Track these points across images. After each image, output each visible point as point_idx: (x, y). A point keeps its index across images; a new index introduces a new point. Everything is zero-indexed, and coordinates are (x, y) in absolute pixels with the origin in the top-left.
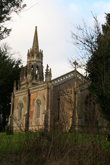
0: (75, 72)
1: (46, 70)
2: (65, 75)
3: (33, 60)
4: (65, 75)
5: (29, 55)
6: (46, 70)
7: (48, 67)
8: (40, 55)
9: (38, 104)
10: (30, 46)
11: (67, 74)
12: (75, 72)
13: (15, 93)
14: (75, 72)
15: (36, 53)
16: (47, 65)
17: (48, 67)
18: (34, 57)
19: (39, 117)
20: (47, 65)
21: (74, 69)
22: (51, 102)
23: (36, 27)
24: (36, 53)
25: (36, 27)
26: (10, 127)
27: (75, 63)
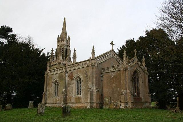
0: (113, 51)
1: (73, 53)
2: (99, 57)
3: (63, 44)
4: (105, 54)
5: (58, 40)
6: (73, 53)
7: (76, 50)
8: (68, 40)
9: (78, 81)
10: (59, 33)
11: (104, 54)
12: (112, 51)
13: (48, 72)
14: (112, 51)
15: (64, 40)
16: (75, 49)
17: (75, 50)
18: (63, 42)
19: (56, 95)
20: (75, 49)
21: (111, 49)
22: (96, 79)
23: (65, 18)
24: (64, 40)
25: (65, 18)
26: (67, 106)
27: (112, 44)
